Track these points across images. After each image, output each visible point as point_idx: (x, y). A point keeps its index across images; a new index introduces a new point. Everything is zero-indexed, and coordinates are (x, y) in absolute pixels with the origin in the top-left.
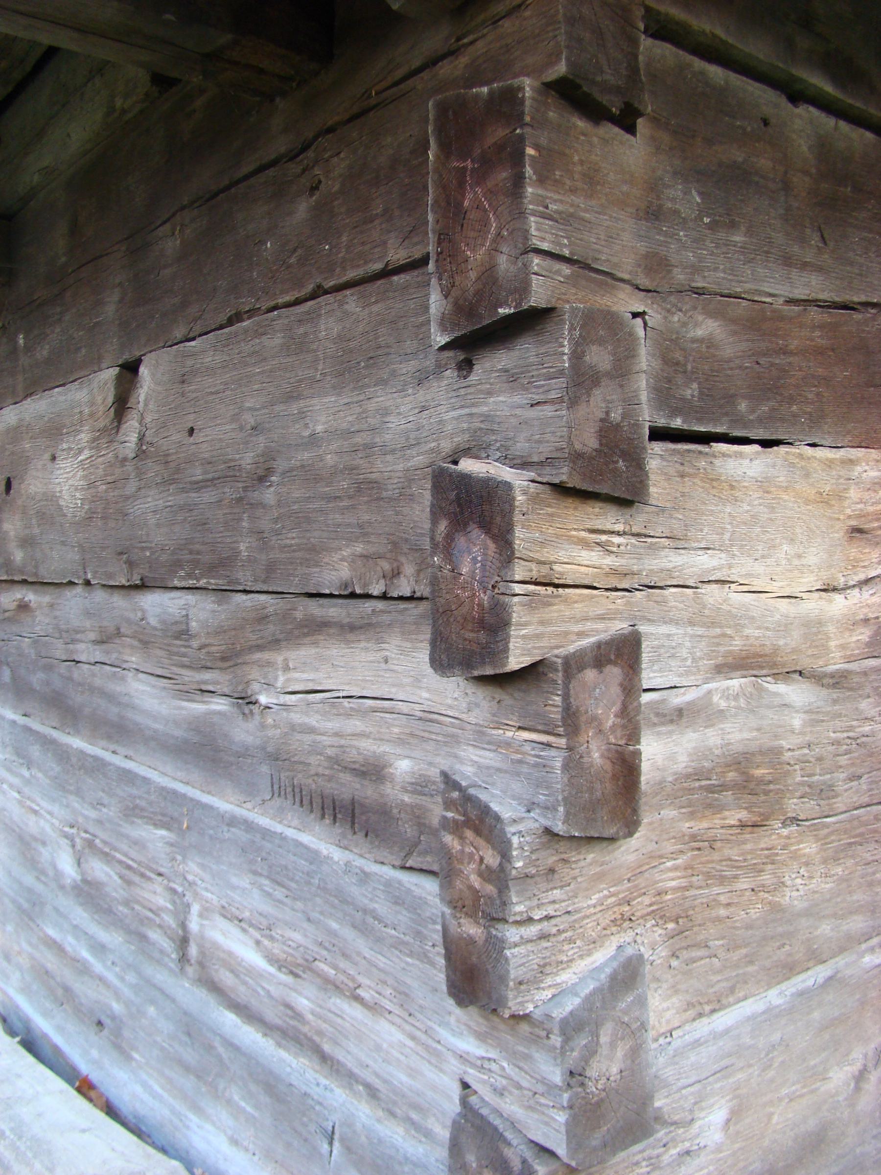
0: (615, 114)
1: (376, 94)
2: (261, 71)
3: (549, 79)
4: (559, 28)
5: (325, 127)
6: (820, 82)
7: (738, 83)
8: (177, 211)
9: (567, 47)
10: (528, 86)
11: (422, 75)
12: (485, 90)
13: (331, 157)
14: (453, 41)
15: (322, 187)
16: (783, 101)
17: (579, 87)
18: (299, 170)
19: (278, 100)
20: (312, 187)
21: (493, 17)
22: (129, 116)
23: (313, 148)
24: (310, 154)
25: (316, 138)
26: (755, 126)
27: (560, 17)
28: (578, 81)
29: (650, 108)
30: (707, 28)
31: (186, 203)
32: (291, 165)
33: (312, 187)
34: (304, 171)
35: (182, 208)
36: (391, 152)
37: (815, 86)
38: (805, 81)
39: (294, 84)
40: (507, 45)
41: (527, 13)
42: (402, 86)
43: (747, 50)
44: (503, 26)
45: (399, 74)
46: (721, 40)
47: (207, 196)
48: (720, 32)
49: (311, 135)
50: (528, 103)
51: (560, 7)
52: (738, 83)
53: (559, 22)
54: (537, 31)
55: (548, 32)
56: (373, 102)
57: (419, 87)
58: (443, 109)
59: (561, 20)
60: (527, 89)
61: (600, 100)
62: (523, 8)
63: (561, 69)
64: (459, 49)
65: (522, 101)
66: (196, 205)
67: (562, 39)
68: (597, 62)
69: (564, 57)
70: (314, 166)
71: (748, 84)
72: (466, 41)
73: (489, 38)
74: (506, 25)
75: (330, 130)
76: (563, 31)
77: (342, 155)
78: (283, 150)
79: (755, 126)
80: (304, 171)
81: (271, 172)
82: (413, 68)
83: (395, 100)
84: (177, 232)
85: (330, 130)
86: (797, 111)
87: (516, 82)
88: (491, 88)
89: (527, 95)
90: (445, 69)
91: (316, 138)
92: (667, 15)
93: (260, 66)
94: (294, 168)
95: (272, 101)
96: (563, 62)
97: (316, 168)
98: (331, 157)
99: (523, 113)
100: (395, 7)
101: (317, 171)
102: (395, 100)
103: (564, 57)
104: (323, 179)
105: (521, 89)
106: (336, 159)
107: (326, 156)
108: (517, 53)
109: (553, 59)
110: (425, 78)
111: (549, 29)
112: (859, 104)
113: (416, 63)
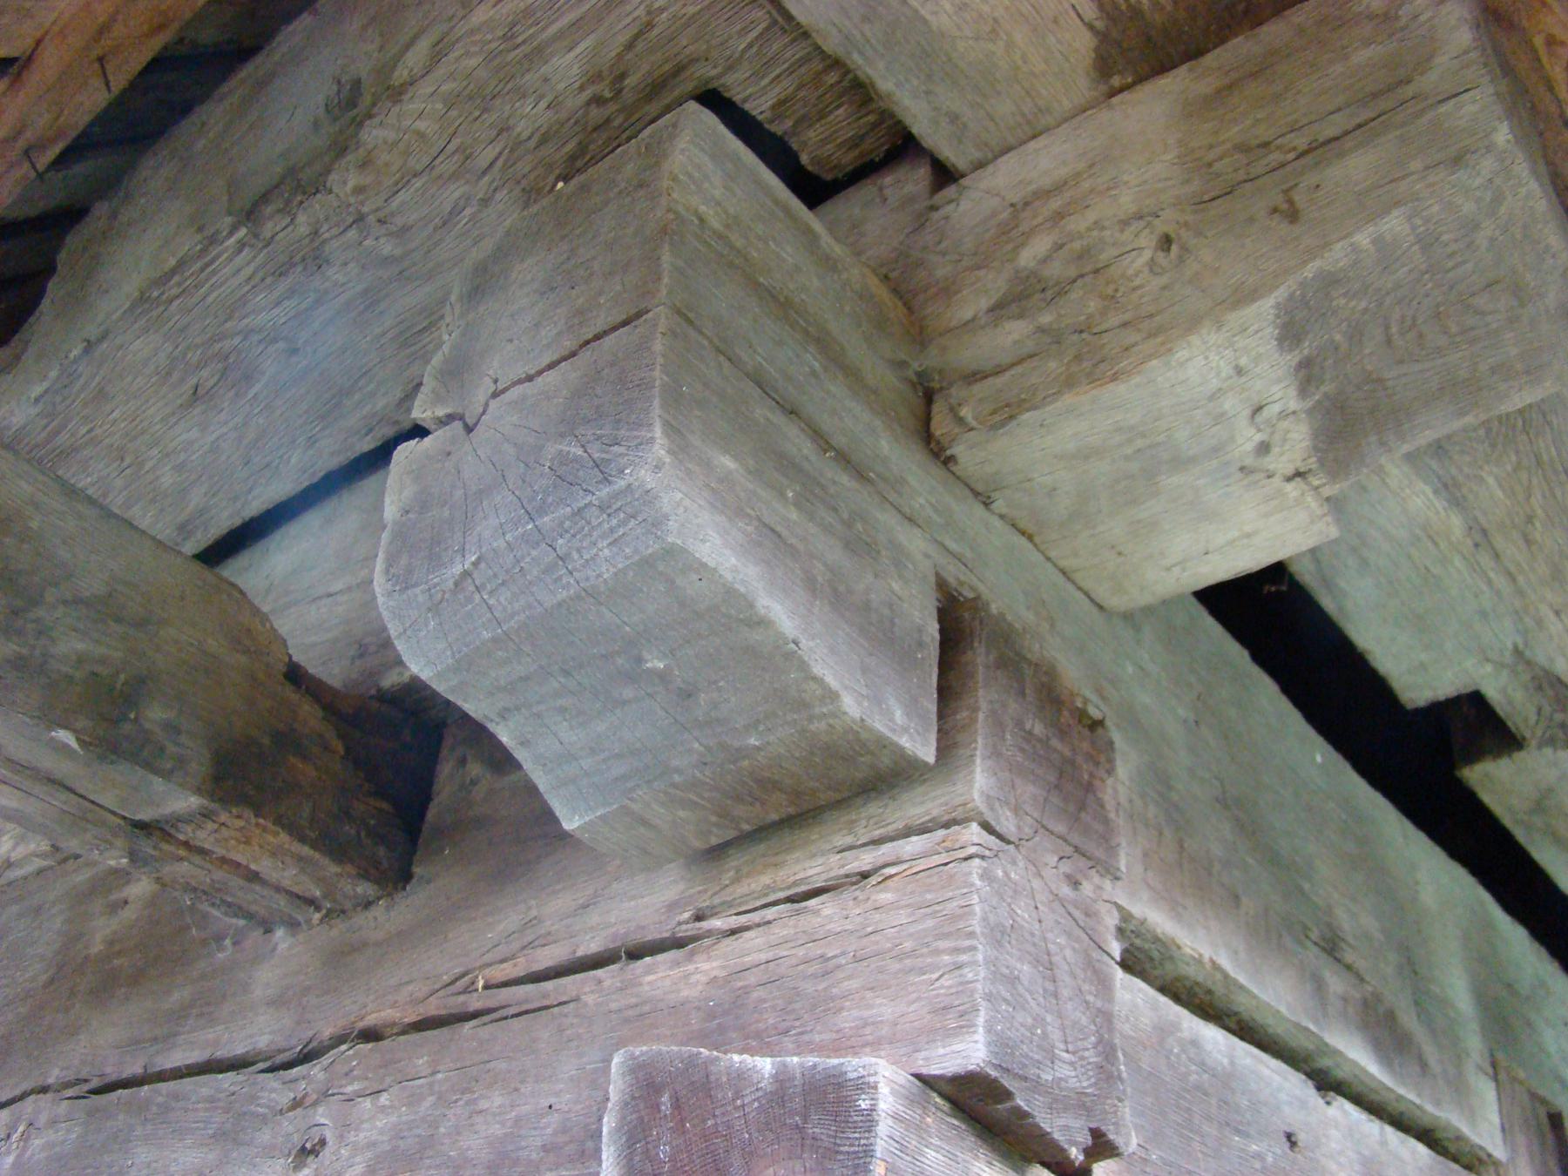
0: (1072, 1162)
1: (486, 987)
2: (254, 877)
3: (935, 1070)
4: (973, 948)
5: (361, 1025)
6: (1356, 1054)
7: (1248, 1061)
8: (32, 1092)
9: (989, 997)
10: (886, 1083)
11: (599, 973)
12: (765, 1065)
13: (362, 1095)
14: (686, 915)
15: (326, 1154)
16: (1308, 1090)
17: (1007, 1095)
18: (285, 1098)
19: (280, 933)
20: (303, 1148)
21: (795, 884)
22: (18, 873)
23: (326, 1060)
24: (316, 1070)
25: (339, 1040)
26: (1279, 1152)
27: (976, 925)
28: (1006, 1082)
29: (1134, 1141)
30: (1207, 953)
31: (51, 1081)
32: (271, 1080)
33: (303, 1148)
34: (296, 1104)
35: (44, 1090)
36: (497, 1130)
37: (1355, 1063)
38: (1340, 1053)
39: (317, 916)
40: (824, 958)
41: (885, 897)
42: (548, 985)
43: (1264, 997)
44: (816, 912)
45: (547, 957)
46: (1226, 976)
47: (95, 1083)
48: (1225, 962)
49: (327, 1032)
50: (884, 1127)
51: (975, 899)
52: (1248, 1061)
53: (971, 935)
54: (908, 945)
55: (937, 952)
56: (475, 1003)
57: (590, 999)
58: (648, 1083)
59: (978, 930)
60: (884, 1089)
61: (1046, 1127)
62: (873, 880)
63: (969, 1052)
64: (695, 939)
65: (869, 1121)
66: (70, 1092)
67: (978, 976)
68: (1045, 1035)
69: (981, 1020)
70: (315, 1104)
71: (1262, 1062)
72: (717, 923)
73: (779, 932)
74: (827, 912)
75: (371, 1035)
76: (980, 957)
77: (384, 1099)
78: (263, 1042)
79: (1279, 1152)
80: (296, 1104)
81: (228, 1080)
82: (580, 953)
83: (527, 1012)
84: (15, 1137)
85: (371, 1035)
86: (1332, 1111)
87: (852, 1065)
88: (785, 1065)
89: (882, 1106)
90: (658, 977)
91: (339, 1040)
92: (1143, 922)
93: (253, 867)
94: (275, 1090)
95: (268, 931)
96: (980, 1035)
97: (321, 1110)
98: (362, 1095)
99: (868, 1152)
100: (570, 824)
101: (321, 1115)
102: (527, 1012)
103: (981, 1020)
104: (329, 1136)
105: (865, 1086)
106: (367, 1103)
107: (349, 1089)
108: (854, 984)
109: (951, 1016)
110: (607, 983)
111: (942, 944)
112: (1411, 1096)
113: (591, 945)
